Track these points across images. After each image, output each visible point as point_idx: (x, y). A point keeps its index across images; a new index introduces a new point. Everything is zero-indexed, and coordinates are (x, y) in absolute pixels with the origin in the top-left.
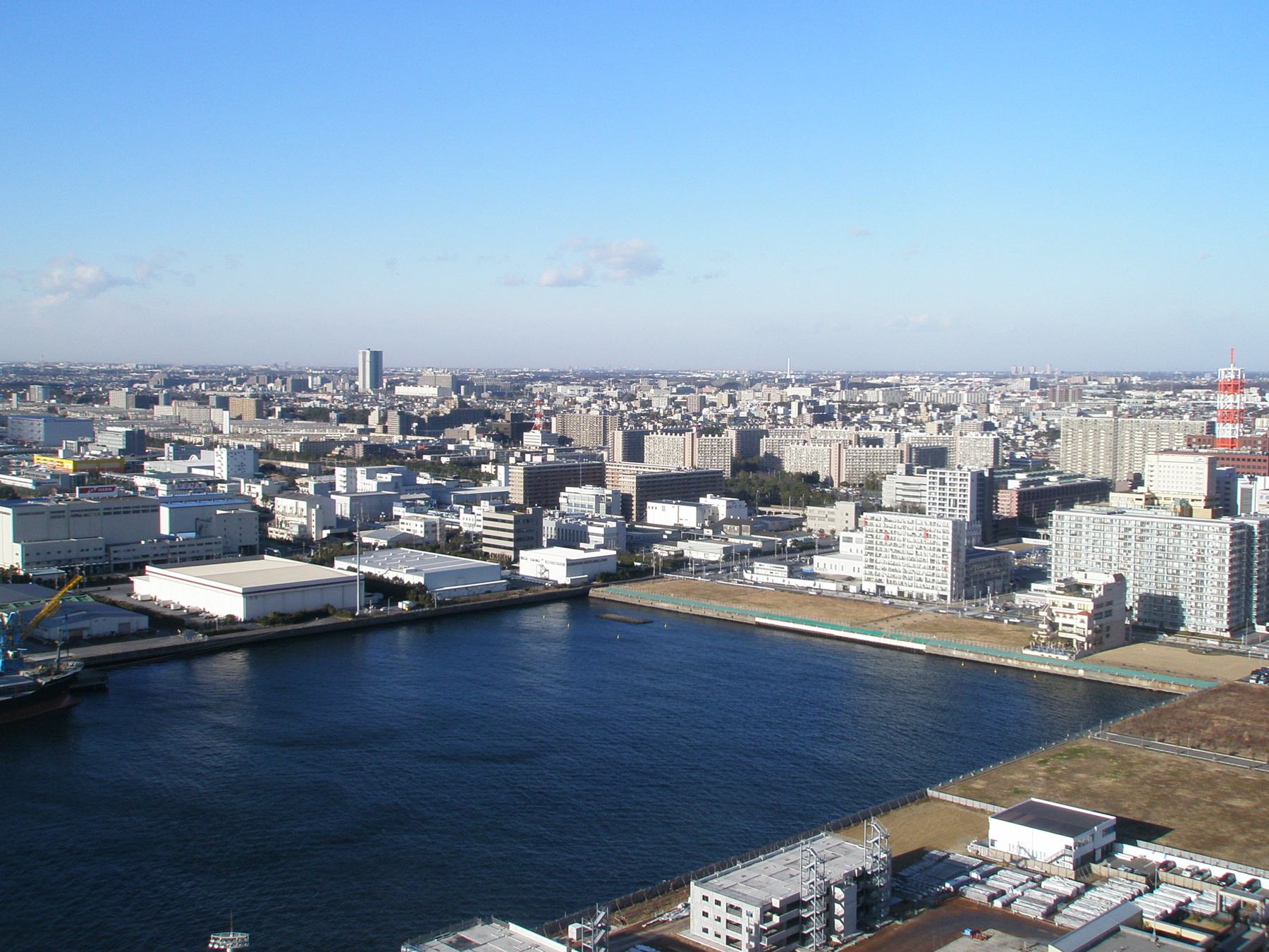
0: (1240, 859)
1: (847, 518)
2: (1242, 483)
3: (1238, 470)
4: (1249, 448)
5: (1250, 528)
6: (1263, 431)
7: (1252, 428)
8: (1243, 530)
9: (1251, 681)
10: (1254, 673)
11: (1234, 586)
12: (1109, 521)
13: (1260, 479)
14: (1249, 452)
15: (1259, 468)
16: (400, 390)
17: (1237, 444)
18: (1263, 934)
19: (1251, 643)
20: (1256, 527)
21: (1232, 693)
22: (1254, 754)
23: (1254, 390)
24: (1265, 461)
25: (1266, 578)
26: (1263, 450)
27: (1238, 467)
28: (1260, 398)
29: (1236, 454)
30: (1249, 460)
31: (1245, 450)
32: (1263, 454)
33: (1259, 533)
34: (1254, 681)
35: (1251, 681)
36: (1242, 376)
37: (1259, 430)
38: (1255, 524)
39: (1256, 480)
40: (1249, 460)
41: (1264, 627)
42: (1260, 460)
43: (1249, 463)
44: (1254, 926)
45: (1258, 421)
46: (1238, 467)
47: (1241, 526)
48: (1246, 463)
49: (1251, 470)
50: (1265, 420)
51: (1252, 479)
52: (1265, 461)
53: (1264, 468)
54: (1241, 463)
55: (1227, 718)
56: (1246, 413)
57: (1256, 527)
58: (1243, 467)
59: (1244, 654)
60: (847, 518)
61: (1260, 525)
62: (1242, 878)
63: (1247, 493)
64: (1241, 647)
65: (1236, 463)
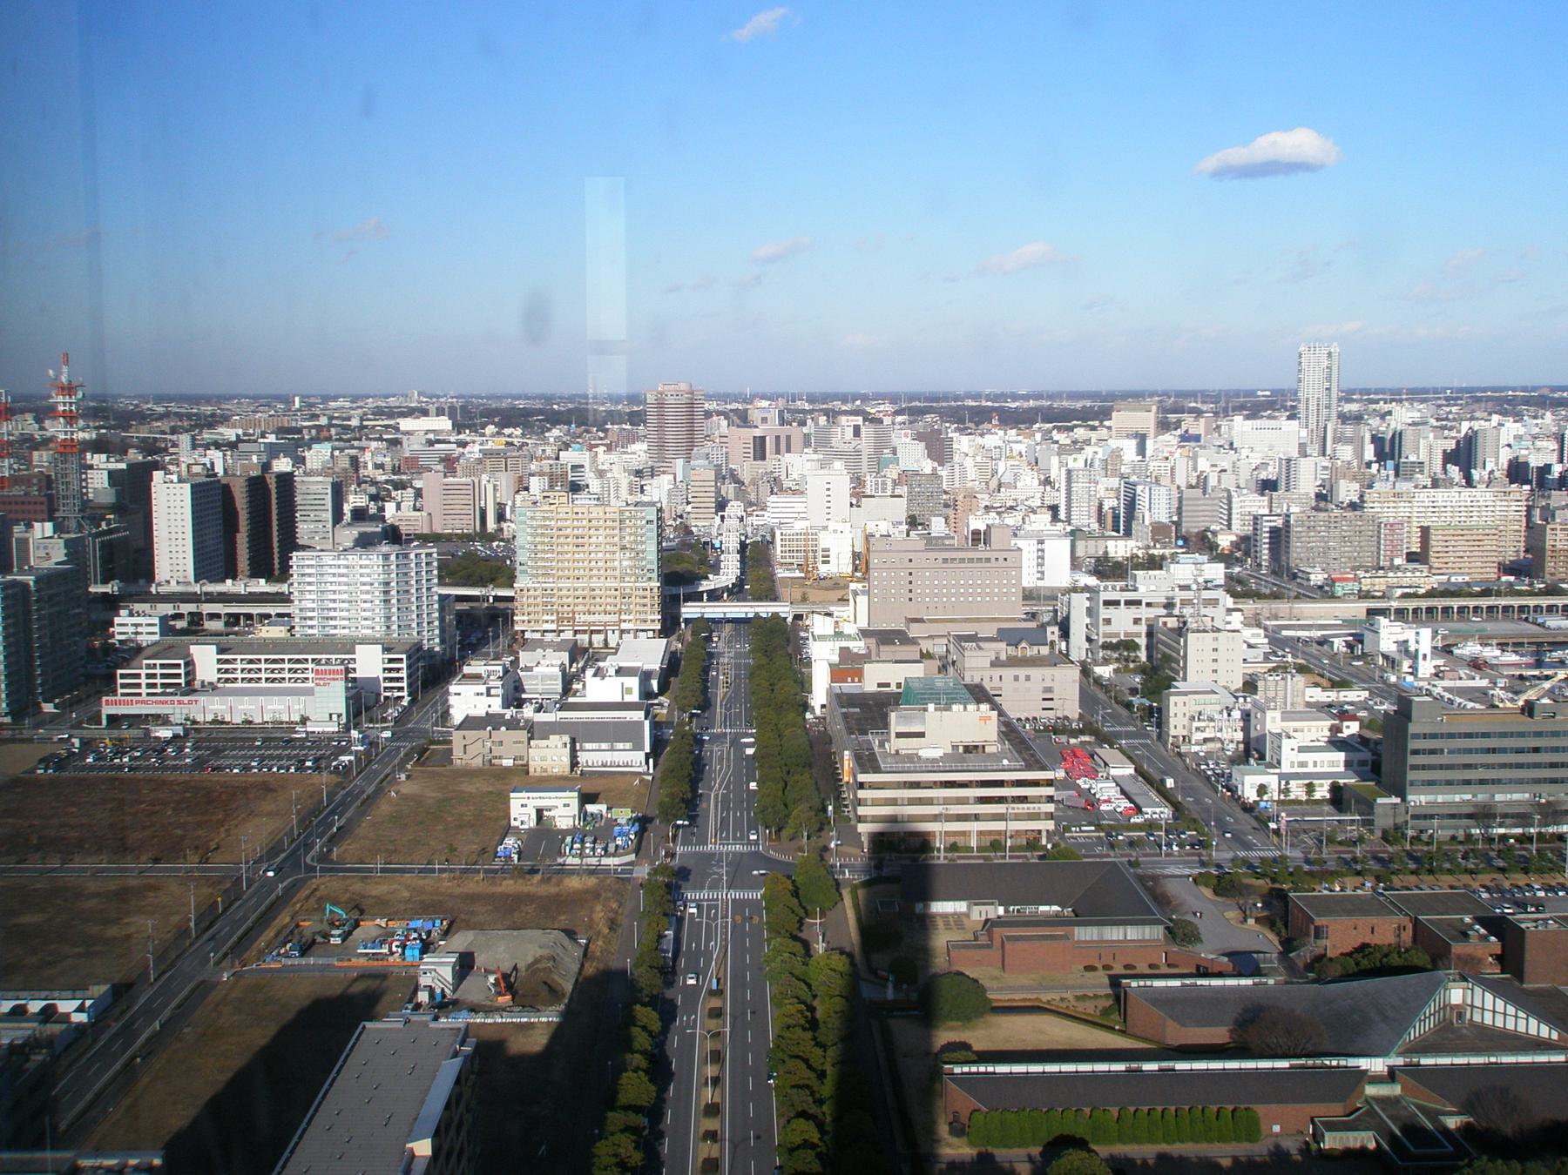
0: (33, 986)
1: (1022, 678)
2: (18, 530)
3: (12, 516)
4: (23, 488)
5: (25, 585)
6: (42, 466)
7: (29, 462)
8: (16, 590)
9: (39, 771)
10: (41, 761)
11: (12, 659)
12: (627, 579)
13: (37, 525)
14: (22, 493)
15: (35, 512)
16: (490, 908)
17: (6, 484)
18: (44, 1060)
19: (37, 726)
20: (32, 583)
21: (17, 790)
22: (44, 858)
23: (29, 417)
24: (42, 503)
25: (49, 645)
26: (39, 490)
27: (10, 512)
28: (37, 426)
29: (9, 496)
30: (23, 503)
31: (18, 491)
32: (39, 495)
33: (37, 591)
34: (42, 771)
35: (39, 771)
36: (6, 398)
37: (37, 466)
38: (30, 580)
39: (32, 527)
40: (23, 503)
41: (52, 705)
42: (35, 503)
43: (23, 507)
44: (35, 1054)
45: (36, 454)
46: (10, 512)
47: (14, 584)
48: (18, 507)
49: (26, 516)
50: (44, 453)
51: (29, 526)
52: (42, 503)
53: (42, 512)
54: (14, 507)
55: (10, 820)
56: (21, 445)
57: (32, 583)
58: (17, 512)
59: (30, 740)
60: (1022, 678)
61: (36, 582)
62: (35, 1006)
63: (24, 543)
64: (24, 732)
65: (9, 507)
